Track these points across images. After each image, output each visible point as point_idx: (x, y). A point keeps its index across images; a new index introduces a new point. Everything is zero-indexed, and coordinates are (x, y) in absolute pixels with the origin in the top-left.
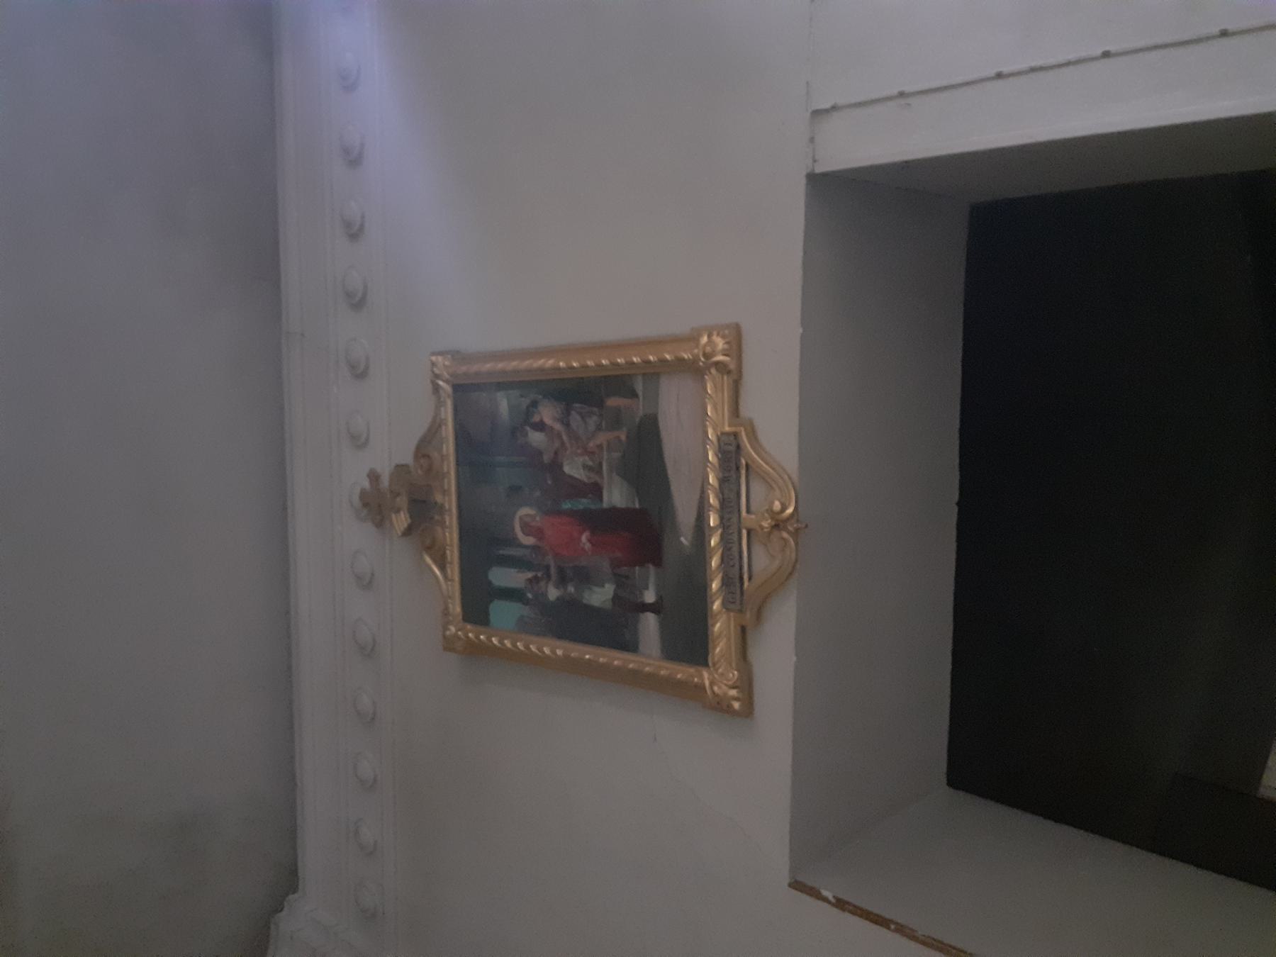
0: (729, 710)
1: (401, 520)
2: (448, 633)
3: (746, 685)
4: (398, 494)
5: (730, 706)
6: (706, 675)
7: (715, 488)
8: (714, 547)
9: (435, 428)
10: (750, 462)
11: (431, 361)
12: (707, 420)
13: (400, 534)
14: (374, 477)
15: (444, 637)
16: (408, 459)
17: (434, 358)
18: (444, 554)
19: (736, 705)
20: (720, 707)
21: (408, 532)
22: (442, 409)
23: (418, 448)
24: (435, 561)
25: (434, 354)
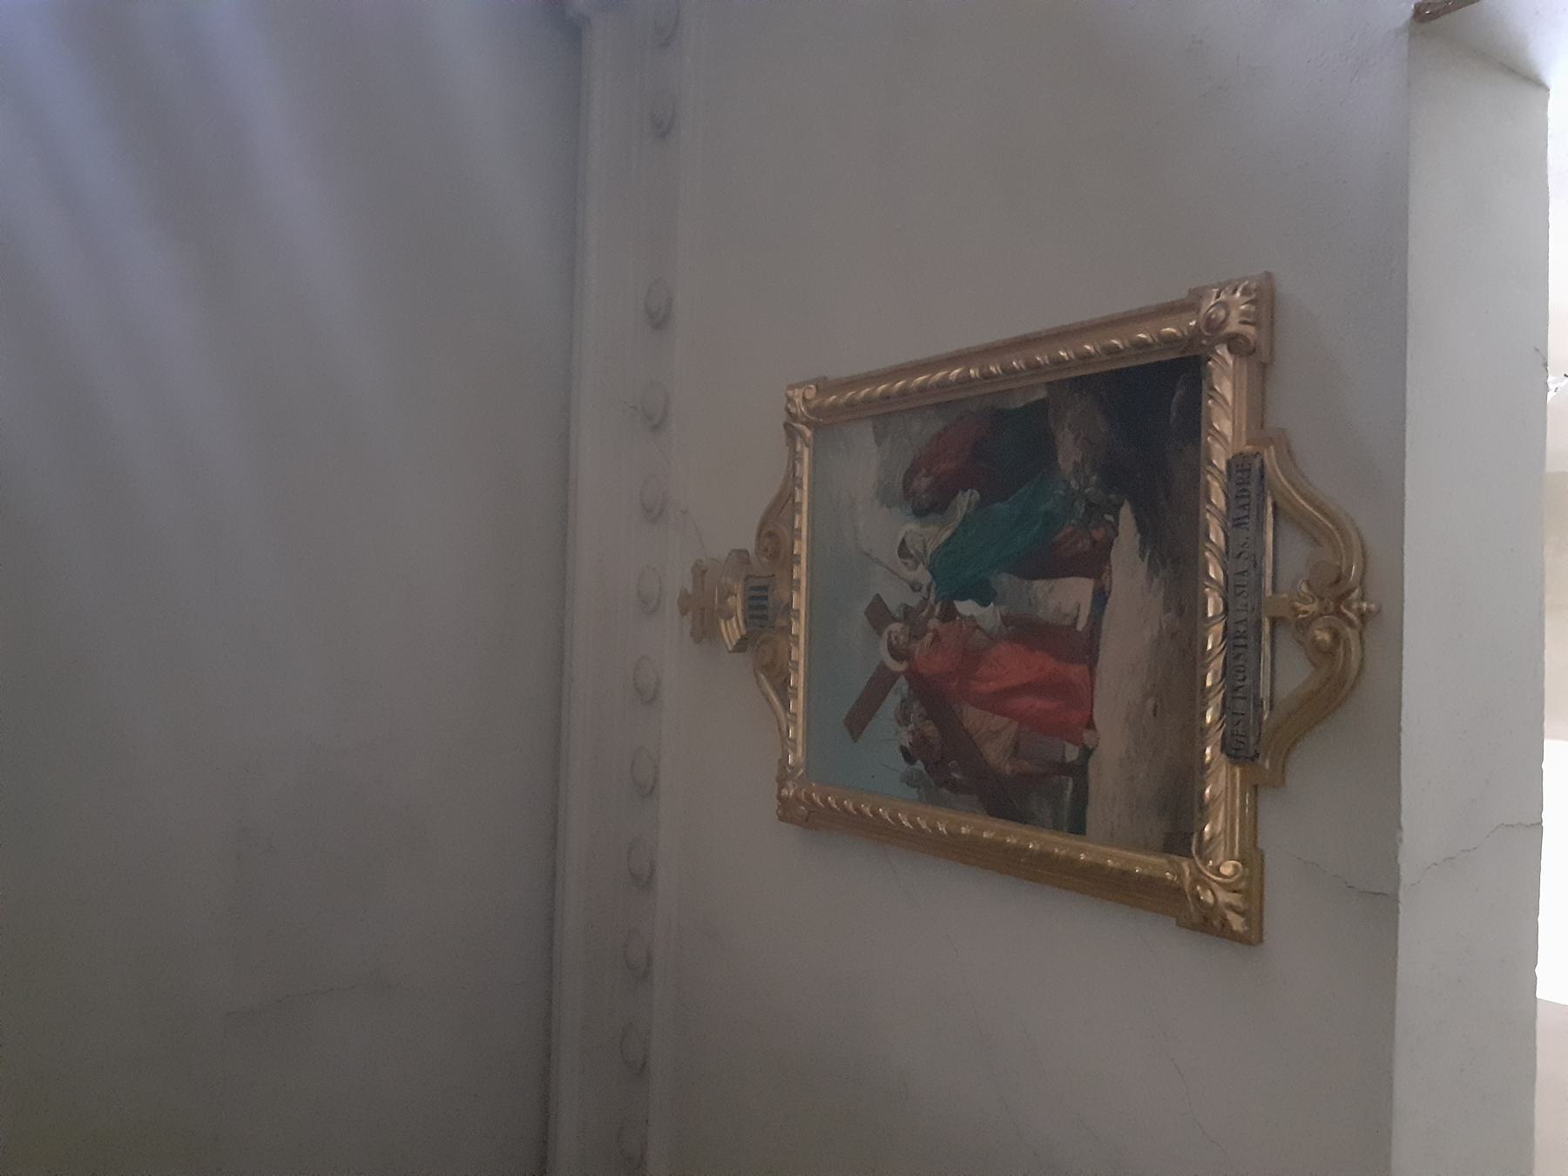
0: (1224, 932)
1: (732, 630)
2: (785, 792)
3: (1252, 887)
4: (731, 593)
5: (1225, 922)
6: (1185, 865)
7: (1220, 511)
8: (1211, 724)
9: (784, 503)
10: (1280, 501)
11: (787, 395)
12: (1209, 472)
13: (730, 648)
14: (700, 572)
15: (779, 798)
16: (749, 544)
17: (790, 393)
18: (787, 681)
19: (1237, 923)
20: (1208, 923)
21: (741, 646)
22: (797, 517)
23: (763, 523)
24: (774, 688)
25: (792, 387)
